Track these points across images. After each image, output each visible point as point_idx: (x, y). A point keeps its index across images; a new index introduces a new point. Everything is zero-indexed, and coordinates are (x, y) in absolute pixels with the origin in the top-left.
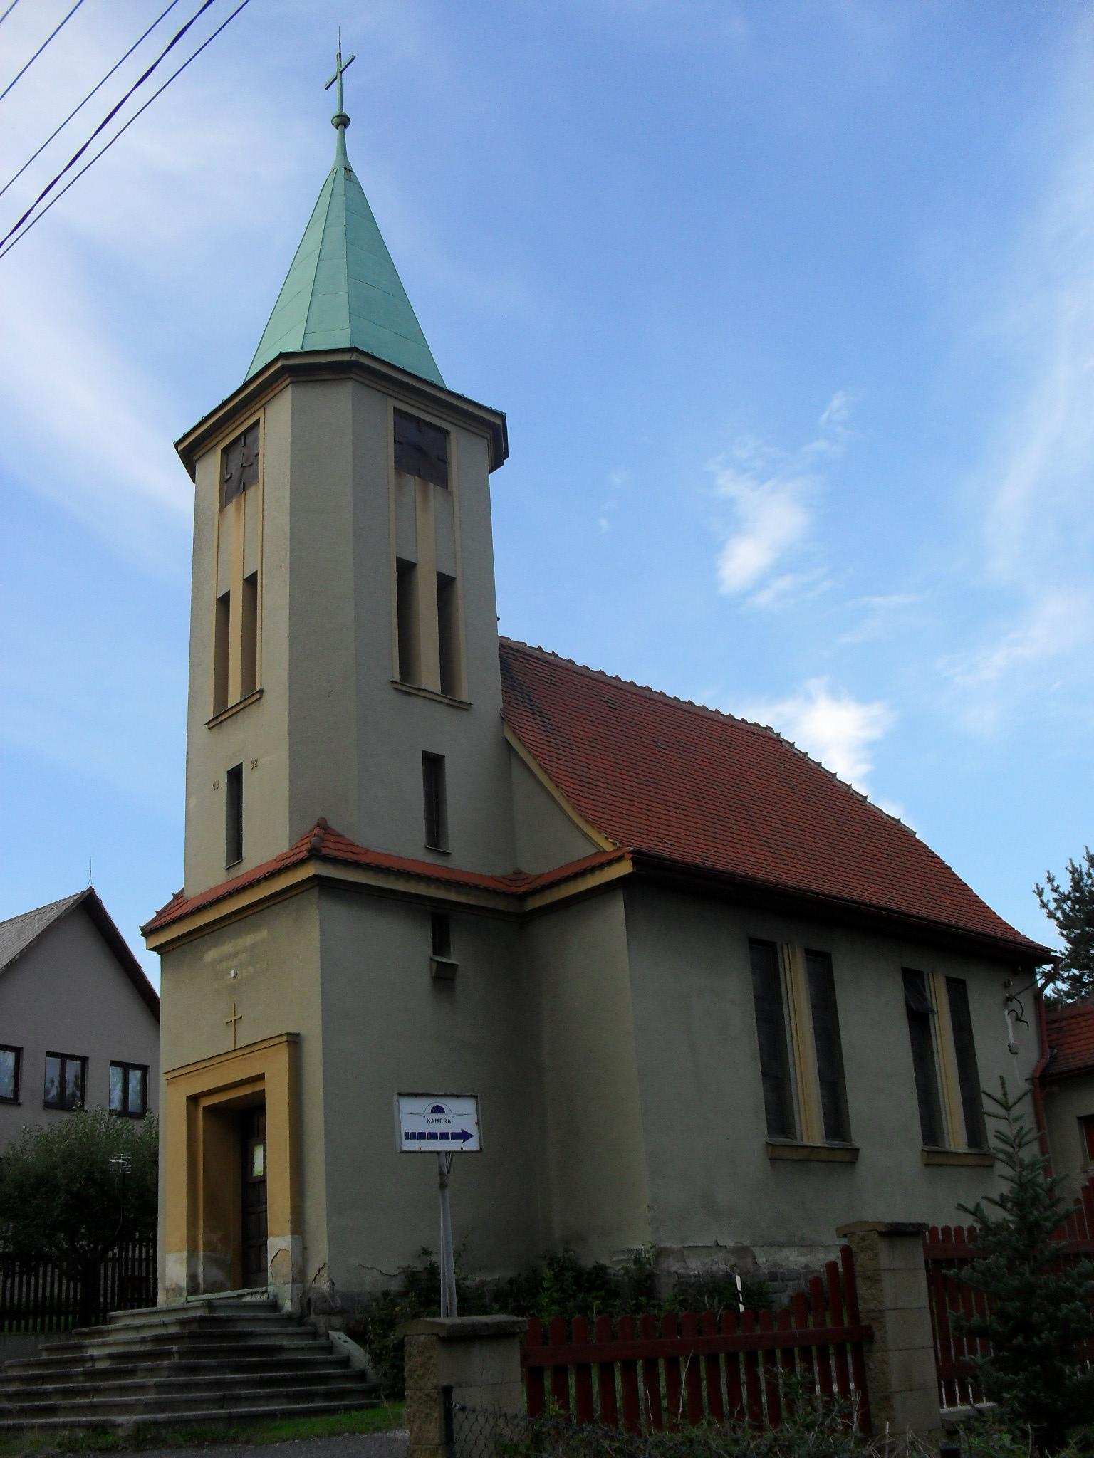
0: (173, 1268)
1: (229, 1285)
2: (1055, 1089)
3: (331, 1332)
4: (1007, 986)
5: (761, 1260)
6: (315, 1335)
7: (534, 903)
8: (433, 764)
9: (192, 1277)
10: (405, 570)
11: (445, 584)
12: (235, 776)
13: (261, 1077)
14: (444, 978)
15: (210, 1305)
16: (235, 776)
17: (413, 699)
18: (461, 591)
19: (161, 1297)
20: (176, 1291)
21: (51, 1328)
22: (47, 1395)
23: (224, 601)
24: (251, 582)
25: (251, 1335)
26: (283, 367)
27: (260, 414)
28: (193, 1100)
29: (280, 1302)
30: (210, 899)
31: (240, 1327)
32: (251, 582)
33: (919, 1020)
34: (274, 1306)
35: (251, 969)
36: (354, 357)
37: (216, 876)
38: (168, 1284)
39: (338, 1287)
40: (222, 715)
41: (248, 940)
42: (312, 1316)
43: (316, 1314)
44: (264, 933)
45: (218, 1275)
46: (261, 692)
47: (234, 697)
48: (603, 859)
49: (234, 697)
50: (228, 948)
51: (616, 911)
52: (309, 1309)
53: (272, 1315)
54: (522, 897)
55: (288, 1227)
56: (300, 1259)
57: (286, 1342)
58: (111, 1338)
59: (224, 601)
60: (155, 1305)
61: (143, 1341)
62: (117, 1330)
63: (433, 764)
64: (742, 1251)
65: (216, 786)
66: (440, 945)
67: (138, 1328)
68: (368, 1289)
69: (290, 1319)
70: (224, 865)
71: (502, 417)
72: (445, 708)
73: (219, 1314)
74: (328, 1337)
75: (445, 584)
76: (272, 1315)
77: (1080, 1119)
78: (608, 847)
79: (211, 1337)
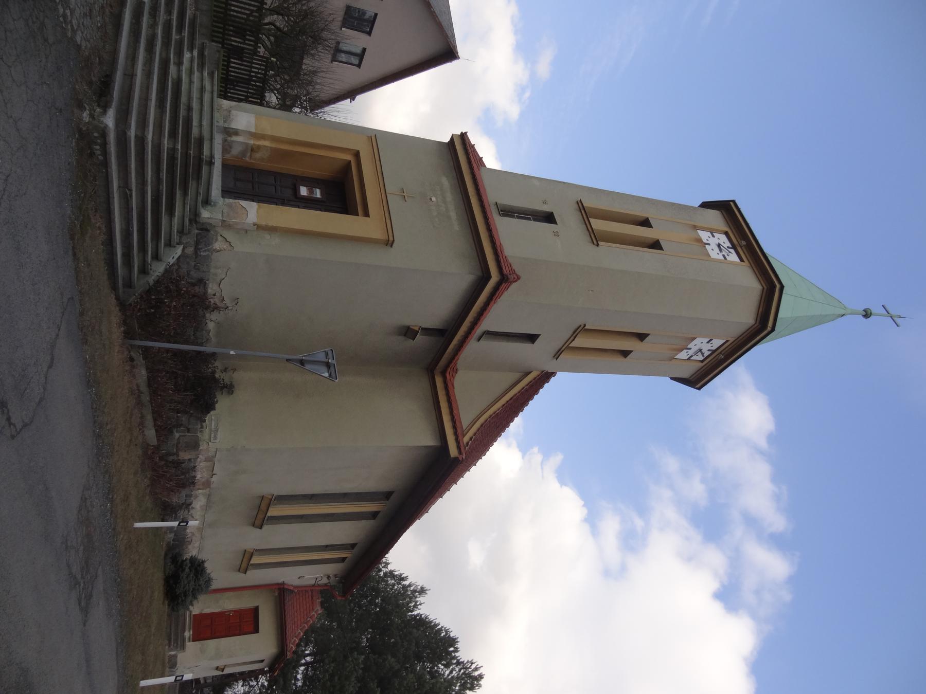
0: (245, 119)
1: (228, 156)
2: (277, 594)
3: (182, 247)
4: (336, 576)
5: (200, 491)
6: (181, 232)
7: (439, 381)
8: (532, 338)
9: (236, 132)
10: (642, 337)
11: (625, 353)
12: (549, 218)
13: (367, 214)
14: (408, 332)
15: (211, 163)
16: (549, 218)
17: (571, 333)
18: (620, 359)
19: (226, 103)
20: (227, 118)
21: (214, 31)
22: (169, 12)
23: (646, 223)
24: (656, 245)
25: (185, 193)
26: (774, 287)
27: (747, 263)
28: (357, 155)
29: (209, 207)
30: (480, 184)
31: (192, 185)
32: (656, 245)
33: (326, 548)
34: (207, 202)
35: (435, 214)
36: (769, 329)
37: (493, 195)
38: (233, 112)
39: (215, 254)
40: (585, 213)
41: (453, 214)
42: (197, 231)
43: (197, 235)
44: (456, 227)
45: (236, 151)
46: (598, 245)
47: (597, 224)
48: (460, 436)
49: (597, 224)
50: (449, 197)
51: (428, 440)
52: (201, 229)
53: (200, 199)
54: (443, 374)
55: (263, 223)
56: (239, 227)
57: (176, 220)
58: (196, 75)
59: (646, 223)
60: (220, 96)
61: (189, 109)
62: (202, 80)
63: (532, 338)
64: (207, 484)
65: (545, 202)
66: (427, 331)
67: (201, 99)
68: (212, 270)
69: (195, 215)
70: (499, 202)
71: (699, 389)
72: (560, 346)
73: (205, 169)
74: (178, 244)
75: (625, 353)
76: (200, 199)
77: (256, 609)
78: (466, 439)
79: (186, 166)
